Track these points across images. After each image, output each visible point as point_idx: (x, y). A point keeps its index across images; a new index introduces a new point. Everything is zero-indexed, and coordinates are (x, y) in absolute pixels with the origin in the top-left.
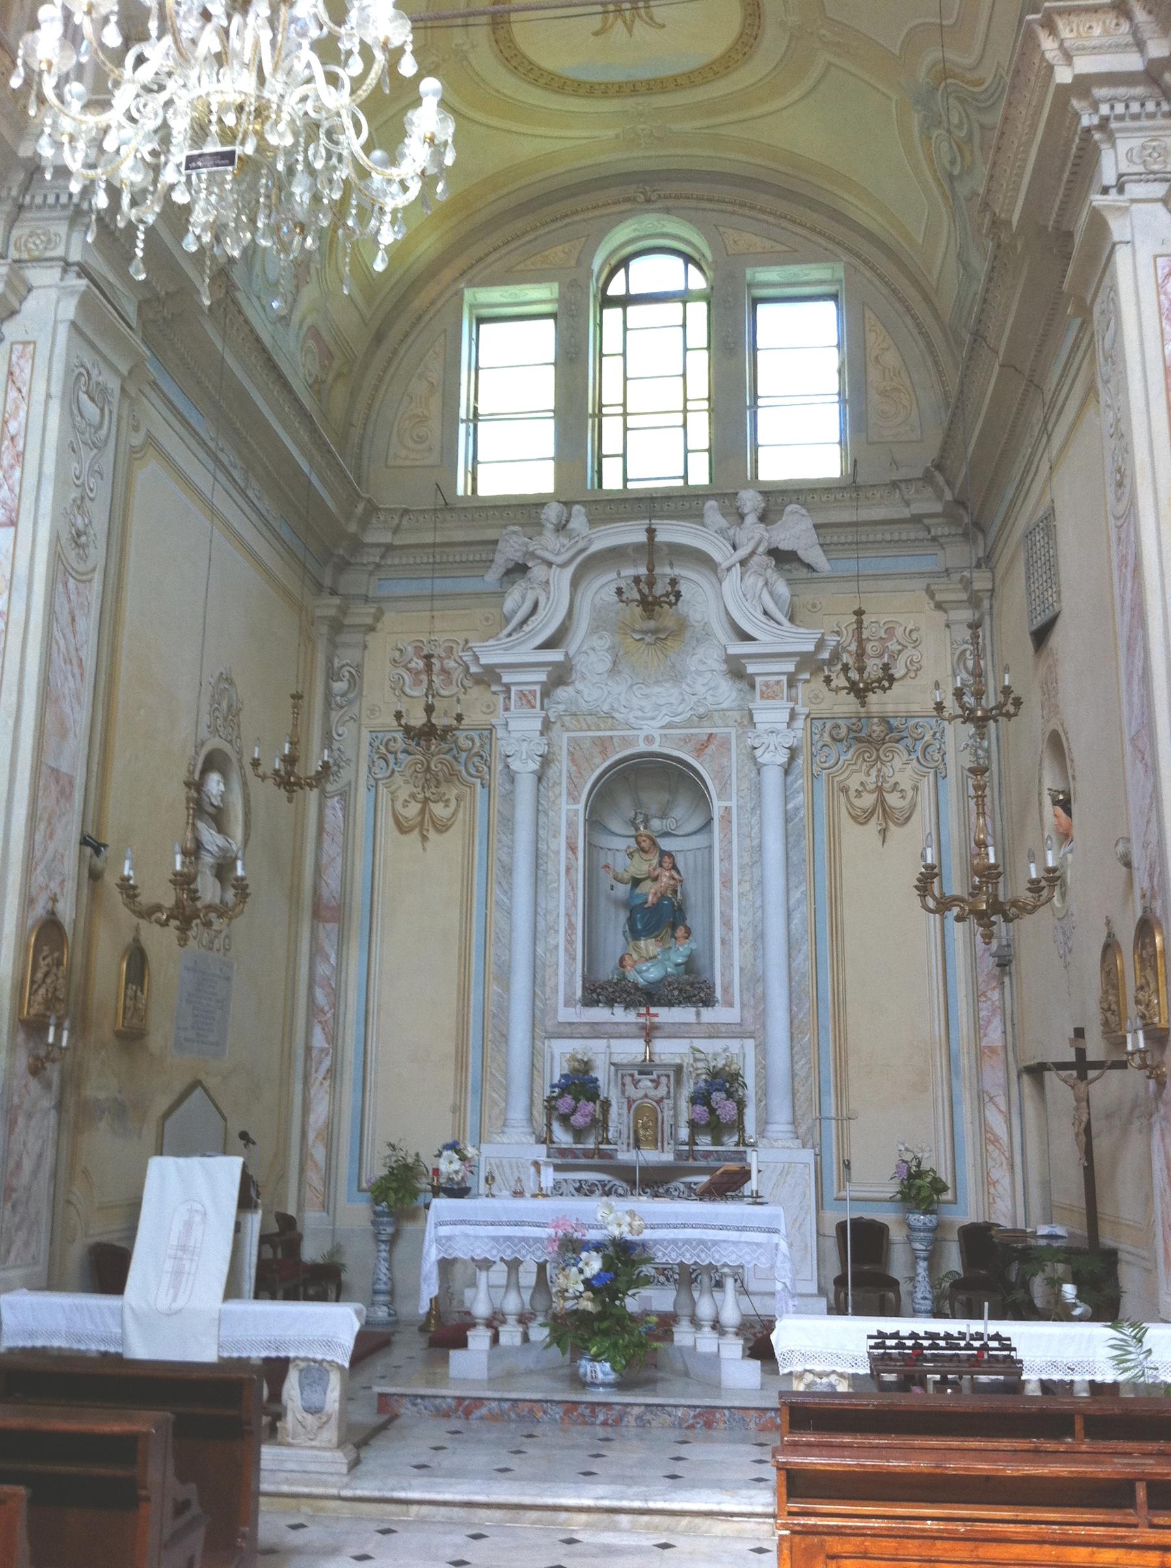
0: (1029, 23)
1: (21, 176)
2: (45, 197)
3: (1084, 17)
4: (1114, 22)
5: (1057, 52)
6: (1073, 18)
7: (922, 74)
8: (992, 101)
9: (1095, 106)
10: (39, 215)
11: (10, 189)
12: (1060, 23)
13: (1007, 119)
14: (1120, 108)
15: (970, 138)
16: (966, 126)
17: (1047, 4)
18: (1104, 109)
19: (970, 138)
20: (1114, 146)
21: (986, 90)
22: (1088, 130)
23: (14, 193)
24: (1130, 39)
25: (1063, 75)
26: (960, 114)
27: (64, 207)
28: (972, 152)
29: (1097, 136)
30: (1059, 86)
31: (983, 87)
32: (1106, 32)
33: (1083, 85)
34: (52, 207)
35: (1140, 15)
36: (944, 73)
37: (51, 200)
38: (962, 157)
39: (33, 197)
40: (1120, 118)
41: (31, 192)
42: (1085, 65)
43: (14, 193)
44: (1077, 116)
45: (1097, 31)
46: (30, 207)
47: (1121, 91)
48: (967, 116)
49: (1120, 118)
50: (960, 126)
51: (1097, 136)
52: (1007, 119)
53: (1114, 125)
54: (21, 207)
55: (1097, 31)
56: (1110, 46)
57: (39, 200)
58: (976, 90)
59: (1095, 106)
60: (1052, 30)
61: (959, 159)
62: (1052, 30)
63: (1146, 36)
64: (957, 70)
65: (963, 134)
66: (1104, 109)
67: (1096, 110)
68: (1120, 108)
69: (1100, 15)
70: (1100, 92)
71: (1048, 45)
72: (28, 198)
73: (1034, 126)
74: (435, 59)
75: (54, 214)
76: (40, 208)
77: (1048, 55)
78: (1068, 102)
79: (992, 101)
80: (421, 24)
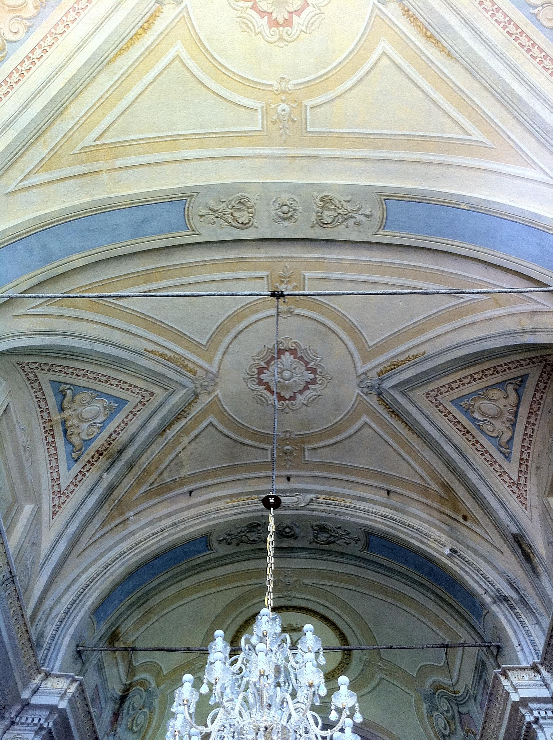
0: (496, 673)
1: (19, 707)
2: (27, 719)
3: (519, 672)
4: (533, 674)
5: (510, 687)
6: (515, 672)
7: (427, 686)
8: (464, 701)
9: (531, 712)
10: (21, 728)
11: (11, 713)
12: (510, 673)
13: (487, 715)
14: (543, 714)
15: (453, 718)
16: (451, 711)
17: (503, 666)
18: (536, 714)
19: (453, 718)
20: (543, 731)
21: (461, 696)
22: (530, 723)
23: (13, 715)
24: (541, 682)
25: (514, 697)
26: (448, 707)
27: (35, 725)
28: (455, 724)
29: (534, 726)
30: (514, 702)
31: (460, 694)
32: (530, 679)
33: (524, 702)
34: (29, 724)
35: (544, 673)
36: (437, 687)
37: (29, 721)
38: (450, 725)
39: (21, 718)
40: (544, 718)
41: (20, 716)
42: (525, 693)
43: (13, 715)
44: (523, 716)
45: (526, 678)
46: (18, 723)
47: (542, 706)
48: (451, 707)
49: (544, 718)
50: (448, 711)
51: (534, 726)
52: (487, 715)
53: (541, 721)
54: (13, 723)
55: (526, 678)
56: (533, 685)
57: (23, 720)
58: (457, 695)
59: (531, 712)
60: (506, 676)
61: (448, 727)
62: (506, 676)
63: (549, 682)
64: (445, 686)
65: (450, 715)
66: (536, 714)
67: (532, 714)
68: (543, 714)
69: (526, 671)
70: (532, 706)
71: (505, 682)
72: (18, 718)
73: (501, 719)
74: (202, 663)
75: (30, 728)
76: (22, 724)
77: (506, 688)
78: (518, 709)
79: (464, 701)
80: (206, 652)
